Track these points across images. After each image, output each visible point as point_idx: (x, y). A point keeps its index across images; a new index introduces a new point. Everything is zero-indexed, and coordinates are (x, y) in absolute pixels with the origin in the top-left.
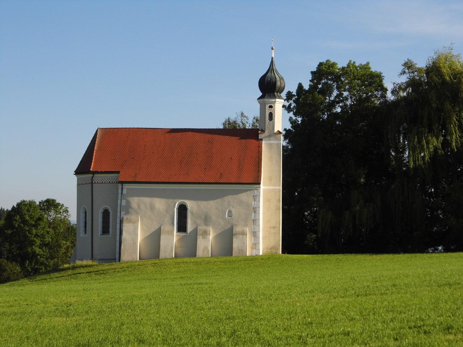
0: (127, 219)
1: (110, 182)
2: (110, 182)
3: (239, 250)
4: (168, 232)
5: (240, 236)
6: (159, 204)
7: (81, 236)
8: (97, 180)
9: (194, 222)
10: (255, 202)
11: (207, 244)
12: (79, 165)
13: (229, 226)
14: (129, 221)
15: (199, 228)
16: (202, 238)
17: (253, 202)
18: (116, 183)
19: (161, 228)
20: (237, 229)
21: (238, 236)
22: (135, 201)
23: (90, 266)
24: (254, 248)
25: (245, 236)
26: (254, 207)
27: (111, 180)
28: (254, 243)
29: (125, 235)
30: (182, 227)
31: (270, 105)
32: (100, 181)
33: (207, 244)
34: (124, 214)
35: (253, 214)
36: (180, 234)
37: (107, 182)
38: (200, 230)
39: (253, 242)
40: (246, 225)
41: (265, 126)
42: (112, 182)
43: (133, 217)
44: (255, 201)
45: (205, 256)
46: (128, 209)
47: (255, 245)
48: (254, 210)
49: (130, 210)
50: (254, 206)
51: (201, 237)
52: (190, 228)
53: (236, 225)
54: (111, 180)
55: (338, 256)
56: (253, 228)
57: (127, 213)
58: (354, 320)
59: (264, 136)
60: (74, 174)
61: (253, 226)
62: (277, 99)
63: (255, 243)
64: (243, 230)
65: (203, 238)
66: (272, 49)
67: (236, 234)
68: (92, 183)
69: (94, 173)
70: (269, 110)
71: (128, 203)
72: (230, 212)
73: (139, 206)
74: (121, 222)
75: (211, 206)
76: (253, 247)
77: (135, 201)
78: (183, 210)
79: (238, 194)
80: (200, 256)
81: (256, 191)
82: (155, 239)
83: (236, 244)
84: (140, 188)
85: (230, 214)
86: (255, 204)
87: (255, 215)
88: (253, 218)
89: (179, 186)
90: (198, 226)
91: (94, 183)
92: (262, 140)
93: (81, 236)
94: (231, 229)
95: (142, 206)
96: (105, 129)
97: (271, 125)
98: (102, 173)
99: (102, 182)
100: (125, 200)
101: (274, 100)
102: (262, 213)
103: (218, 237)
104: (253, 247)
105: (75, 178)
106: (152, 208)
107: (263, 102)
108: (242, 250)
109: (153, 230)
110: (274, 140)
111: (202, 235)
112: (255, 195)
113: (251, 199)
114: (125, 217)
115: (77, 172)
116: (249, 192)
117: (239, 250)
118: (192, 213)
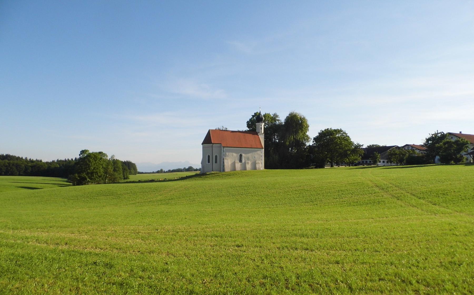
9: (245, 160)
11: (249, 166)
20: (257, 162)
29: (225, 163)
30: (241, 161)
33: (249, 166)
43: (227, 158)
52: (243, 161)
57: (225, 156)
71: (225, 154)
74: (223, 159)
75: (250, 155)
78: (241, 156)
82: (234, 164)
83: (257, 166)
102: (259, 157)
103: (251, 164)
105: (202, 146)
106: (233, 155)
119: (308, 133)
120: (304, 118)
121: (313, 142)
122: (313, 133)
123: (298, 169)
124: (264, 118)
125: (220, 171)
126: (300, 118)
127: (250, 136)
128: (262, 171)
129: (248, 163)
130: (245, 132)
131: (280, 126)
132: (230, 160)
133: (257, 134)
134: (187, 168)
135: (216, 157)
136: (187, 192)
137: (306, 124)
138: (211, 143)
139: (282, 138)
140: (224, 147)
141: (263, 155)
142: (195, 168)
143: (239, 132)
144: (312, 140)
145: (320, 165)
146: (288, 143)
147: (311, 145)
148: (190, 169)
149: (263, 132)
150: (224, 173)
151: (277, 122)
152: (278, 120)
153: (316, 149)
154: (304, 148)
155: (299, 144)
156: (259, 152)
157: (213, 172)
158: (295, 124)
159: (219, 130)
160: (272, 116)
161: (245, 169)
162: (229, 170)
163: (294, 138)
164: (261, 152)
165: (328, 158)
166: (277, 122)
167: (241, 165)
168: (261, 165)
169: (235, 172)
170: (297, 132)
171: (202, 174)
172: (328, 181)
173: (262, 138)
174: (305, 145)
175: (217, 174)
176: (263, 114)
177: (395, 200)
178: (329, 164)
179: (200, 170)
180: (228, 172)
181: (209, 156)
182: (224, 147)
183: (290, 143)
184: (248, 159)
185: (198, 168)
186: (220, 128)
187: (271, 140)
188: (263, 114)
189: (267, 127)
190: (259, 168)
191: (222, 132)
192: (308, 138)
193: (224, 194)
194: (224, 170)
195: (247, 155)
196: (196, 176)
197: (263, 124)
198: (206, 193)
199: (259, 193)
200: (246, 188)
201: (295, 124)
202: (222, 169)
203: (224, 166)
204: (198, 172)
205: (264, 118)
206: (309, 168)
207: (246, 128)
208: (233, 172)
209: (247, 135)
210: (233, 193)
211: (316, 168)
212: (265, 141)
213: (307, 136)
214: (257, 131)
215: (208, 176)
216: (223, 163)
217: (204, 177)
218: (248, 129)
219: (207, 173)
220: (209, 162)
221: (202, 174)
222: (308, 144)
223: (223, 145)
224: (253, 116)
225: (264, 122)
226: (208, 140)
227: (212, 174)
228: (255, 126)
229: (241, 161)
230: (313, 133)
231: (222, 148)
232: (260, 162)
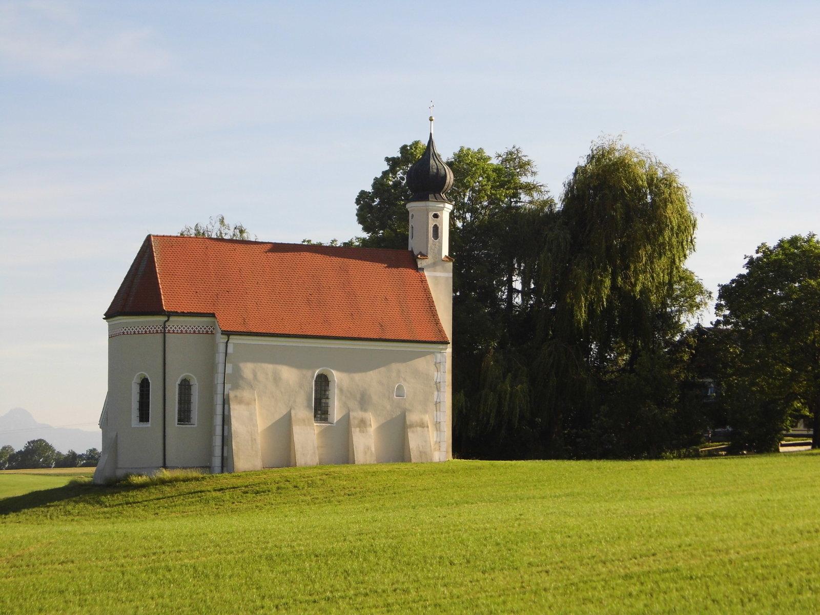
0: (236, 396)
1: (207, 332)
2: (207, 332)
3: (420, 452)
4: (304, 420)
5: (419, 429)
6: (289, 374)
7: (132, 426)
8: (173, 328)
9: (344, 405)
10: (439, 373)
11: (366, 443)
12: (113, 303)
13: (398, 412)
14: (240, 401)
15: (352, 414)
16: (360, 431)
17: (436, 373)
18: (156, 333)
19: (291, 414)
20: (412, 418)
21: (415, 429)
22: (247, 369)
23: (197, 479)
24: (436, 449)
25: (426, 429)
26: (436, 382)
27: (209, 329)
28: (436, 441)
29: (236, 425)
30: (321, 410)
31: (435, 213)
32: (190, 329)
33: (366, 443)
34: (230, 389)
35: (436, 393)
36: (321, 424)
37: (153, 331)
38: (354, 418)
39: (435, 440)
40: (426, 412)
41: (427, 247)
42: (199, 331)
43: (246, 394)
44: (438, 371)
45: (368, 462)
46: (237, 380)
47: (783, 445)
48: (437, 388)
49: (241, 382)
50: (437, 380)
51: (358, 429)
52: (336, 412)
53: (410, 411)
54: (201, 328)
55: (737, 465)
56: (435, 416)
57: (236, 387)
58: (712, 564)
59: (425, 264)
60: (104, 319)
61: (435, 412)
62: (446, 204)
63: (438, 440)
64: (422, 420)
65: (361, 431)
66: (431, 120)
67: (411, 426)
68: (165, 333)
69: (170, 314)
70: (434, 220)
71: (237, 371)
72: (400, 388)
73: (255, 375)
74: (226, 402)
75: (371, 380)
76: (436, 448)
77: (247, 369)
78: (323, 382)
79: (411, 359)
80: (362, 463)
81: (439, 355)
82: (283, 430)
83: (414, 441)
84: (331, 348)
85: (400, 392)
86: (439, 376)
87: (438, 395)
88: (435, 400)
89: (283, 341)
90: (291, 409)
91: (166, 332)
92: (422, 269)
93: (132, 426)
94: (403, 417)
95: (261, 376)
96: (161, 236)
97: (437, 247)
98: (183, 314)
99: (182, 331)
100: (231, 365)
101: (442, 205)
102: (426, 390)
103: (382, 428)
104: (436, 448)
105: (105, 324)
106: (277, 379)
107: (425, 208)
108: (425, 453)
109: (278, 416)
110: (440, 272)
111: (359, 426)
112: (438, 361)
113: (433, 368)
114: (232, 395)
115: (109, 315)
116: (428, 357)
117: (420, 452)
118: (341, 390)
119: (692, 263)
120: (668, 181)
121: (718, 307)
122: (715, 259)
123: (638, 457)
124: (450, 177)
125: (207, 468)
126: (650, 181)
127: (376, 275)
128: (440, 470)
129: (363, 424)
130: (347, 251)
131: (542, 218)
132: (262, 405)
133: (412, 261)
134: (19, 446)
135: (185, 386)
136: (22, 581)
137: (681, 212)
138: (155, 309)
139: (555, 284)
140: (228, 334)
141: (448, 378)
142: (63, 448)
143: (318, 249)
144: (714, 301)
145: (755, 437)
146: (582, 315)
147: (706, 324)
148: (35, 455)
149: (445, 251)
150: (225, 479)
151: (524, 198)
152: (529, 188)
153: (735, 350)
154: (668, 343)
155: (642, 319)
156: (422, 364)
157: (166, 474)
158: (620, 210)
159: (201, 237)
160: (495, 162)
161: (347, 457)
162: (258, 464)
163: (614, 287)
164: (437, 365)
165: (794, 396)
166: (524, 198)
167: (323, 433)
168: (432, 436)
169: (286, 472)
170: (622, 260)
171: (104, 484)
172: (800, 524)
173: (439, 284)
174: (677, 327)
175: (193, 486)
176: (446, 152)
177: (239, 504)
178: (801, 428)
179: (91, 459)
180: (248, 473)
181: (144, 385)
182: (228, 334)
183: (591, 312)
184: (364, 401)
185: (81, 450)
186: (204, 225)
187: (489, 295)
188: (446, 152)
189: (467, 227)
190: (422, 453)
191: (219, 254)
192: (692, 292)
193: (228, 595)
194: (226, 464)
195: (357, 377)
196: (74, 492)
197: (449, 207)
198: (129, 587)
199: (428, 594)
200: (352, 565)
201: (620, 210)
202: (217, 456)
203: (226, 440)
204: (85, 474)
205: (450, 177)
206: (697, 456)
207: (349, 230)
208: (276, 475)
209: (352, 263)
210: (284, 590)
211: (734, 451)
212: (457, 304)
213: (686, 278)
214: (414, 244)
215: (140, 495)
216: (226, 420)
217: (119, 498)
218: (366, 236)
219: (136, 480)
220: (144, 416)
221: (104, 484)
222: (689, 321)
223: (225, 321)
224: (394, 163)
225: (454, 196)
226: (139, 295)
227: (163, 482)
228: (404, 216)
229: (321, 410)
230: (715, 259)
231: (221, 339)
232: (427, 418)
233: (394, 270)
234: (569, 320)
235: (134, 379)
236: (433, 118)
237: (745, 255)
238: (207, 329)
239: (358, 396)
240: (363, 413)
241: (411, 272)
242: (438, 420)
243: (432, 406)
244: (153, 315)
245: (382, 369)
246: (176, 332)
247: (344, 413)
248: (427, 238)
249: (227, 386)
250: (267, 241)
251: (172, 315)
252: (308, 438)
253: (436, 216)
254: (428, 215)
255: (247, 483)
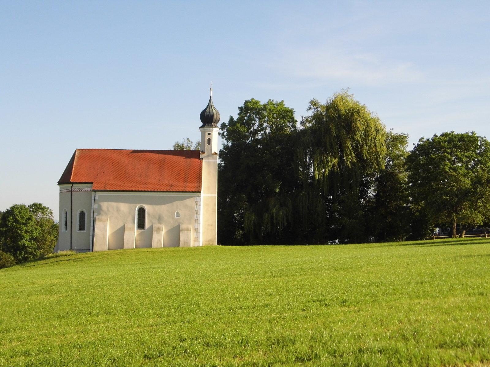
5: (186, 232)
6: (124, 207)
11: (160, 238)
13: (177, 224)
14: (100, 220)
16: (157, 233)
17: (196, 206)
20: (183, 226)
21: (184, 232)
22: (105, 205)
25: (189, 232)
30: (141, 225)
32: (78, 189)
33: (160, 238)
35: (196, 215)
38: (155, 227)
40: (190, 223)
43: (103, 217)
46: (99, 211)
48: (196, 212)
49: (101, 212)
51: (156, 232)
52: (147, 225)
57: (99, 214)
61: (195, 224)
65: (157, 233)
66: (211, 90)
67: (182, 230)
68: (71, 191)
69: (73, 183)
72: (178, 213)
73: (108, 209)
74: (94, 221)
75: (163, 209)
77: (105, 205)
78: (142, 212)
81: (197, 198)
82: (120, 233)
88: (195, 218)
90: (153, 224)
92: (202, 159)
94: (179, 226)
101: (211, 129)
105: (58, 187)
106: (118, 210)
108: (187, 243)
109: (119, 227)
111: (157, 231)
112: (197, 200)
113: (194, 203)
114: (97, 217)
116: (192, 199)
118: (149, 214)
129: (159, 230)
167: (140, 234)
215: (47, 261)
229: (141, 225)
233: (188, 160)
234: (298, 181)
235: (63, 211)
236: (212, 89)
237: (413, 143)
238: (85, 189)
239: (157, 217)
240: (159, 224)
241: (196, 160)
242: (197, 228)
243: (193, 221)
244: (67, 184)
245: (169, 205)
246: (77, 191)
247: (150, 225)
248: (205, 144)
249: (95, 214)
250: (122, 149)
251: (74, 184)
252: (133, 235)
253: (209, 134)
254: (205, 134)
255: (80, 257)
